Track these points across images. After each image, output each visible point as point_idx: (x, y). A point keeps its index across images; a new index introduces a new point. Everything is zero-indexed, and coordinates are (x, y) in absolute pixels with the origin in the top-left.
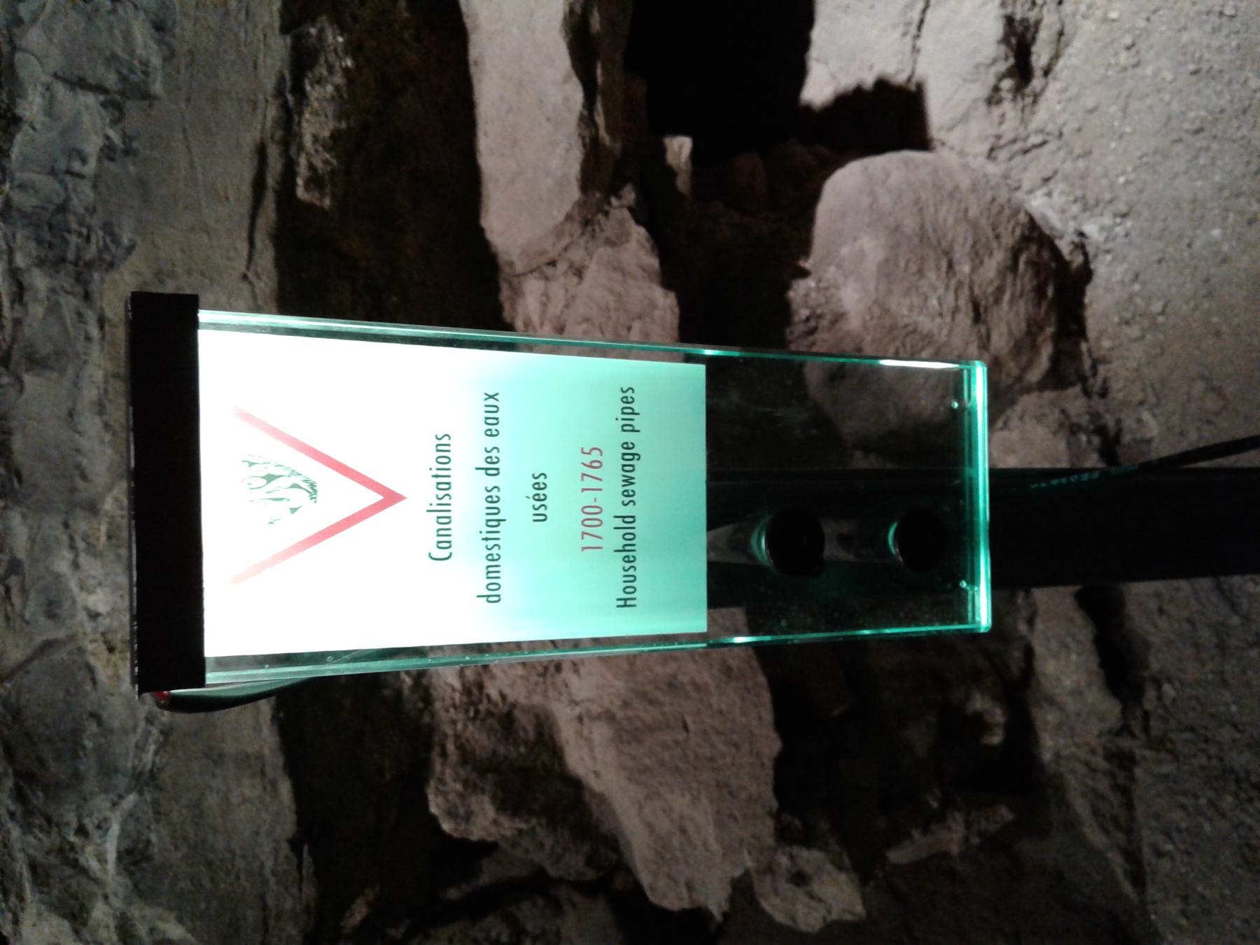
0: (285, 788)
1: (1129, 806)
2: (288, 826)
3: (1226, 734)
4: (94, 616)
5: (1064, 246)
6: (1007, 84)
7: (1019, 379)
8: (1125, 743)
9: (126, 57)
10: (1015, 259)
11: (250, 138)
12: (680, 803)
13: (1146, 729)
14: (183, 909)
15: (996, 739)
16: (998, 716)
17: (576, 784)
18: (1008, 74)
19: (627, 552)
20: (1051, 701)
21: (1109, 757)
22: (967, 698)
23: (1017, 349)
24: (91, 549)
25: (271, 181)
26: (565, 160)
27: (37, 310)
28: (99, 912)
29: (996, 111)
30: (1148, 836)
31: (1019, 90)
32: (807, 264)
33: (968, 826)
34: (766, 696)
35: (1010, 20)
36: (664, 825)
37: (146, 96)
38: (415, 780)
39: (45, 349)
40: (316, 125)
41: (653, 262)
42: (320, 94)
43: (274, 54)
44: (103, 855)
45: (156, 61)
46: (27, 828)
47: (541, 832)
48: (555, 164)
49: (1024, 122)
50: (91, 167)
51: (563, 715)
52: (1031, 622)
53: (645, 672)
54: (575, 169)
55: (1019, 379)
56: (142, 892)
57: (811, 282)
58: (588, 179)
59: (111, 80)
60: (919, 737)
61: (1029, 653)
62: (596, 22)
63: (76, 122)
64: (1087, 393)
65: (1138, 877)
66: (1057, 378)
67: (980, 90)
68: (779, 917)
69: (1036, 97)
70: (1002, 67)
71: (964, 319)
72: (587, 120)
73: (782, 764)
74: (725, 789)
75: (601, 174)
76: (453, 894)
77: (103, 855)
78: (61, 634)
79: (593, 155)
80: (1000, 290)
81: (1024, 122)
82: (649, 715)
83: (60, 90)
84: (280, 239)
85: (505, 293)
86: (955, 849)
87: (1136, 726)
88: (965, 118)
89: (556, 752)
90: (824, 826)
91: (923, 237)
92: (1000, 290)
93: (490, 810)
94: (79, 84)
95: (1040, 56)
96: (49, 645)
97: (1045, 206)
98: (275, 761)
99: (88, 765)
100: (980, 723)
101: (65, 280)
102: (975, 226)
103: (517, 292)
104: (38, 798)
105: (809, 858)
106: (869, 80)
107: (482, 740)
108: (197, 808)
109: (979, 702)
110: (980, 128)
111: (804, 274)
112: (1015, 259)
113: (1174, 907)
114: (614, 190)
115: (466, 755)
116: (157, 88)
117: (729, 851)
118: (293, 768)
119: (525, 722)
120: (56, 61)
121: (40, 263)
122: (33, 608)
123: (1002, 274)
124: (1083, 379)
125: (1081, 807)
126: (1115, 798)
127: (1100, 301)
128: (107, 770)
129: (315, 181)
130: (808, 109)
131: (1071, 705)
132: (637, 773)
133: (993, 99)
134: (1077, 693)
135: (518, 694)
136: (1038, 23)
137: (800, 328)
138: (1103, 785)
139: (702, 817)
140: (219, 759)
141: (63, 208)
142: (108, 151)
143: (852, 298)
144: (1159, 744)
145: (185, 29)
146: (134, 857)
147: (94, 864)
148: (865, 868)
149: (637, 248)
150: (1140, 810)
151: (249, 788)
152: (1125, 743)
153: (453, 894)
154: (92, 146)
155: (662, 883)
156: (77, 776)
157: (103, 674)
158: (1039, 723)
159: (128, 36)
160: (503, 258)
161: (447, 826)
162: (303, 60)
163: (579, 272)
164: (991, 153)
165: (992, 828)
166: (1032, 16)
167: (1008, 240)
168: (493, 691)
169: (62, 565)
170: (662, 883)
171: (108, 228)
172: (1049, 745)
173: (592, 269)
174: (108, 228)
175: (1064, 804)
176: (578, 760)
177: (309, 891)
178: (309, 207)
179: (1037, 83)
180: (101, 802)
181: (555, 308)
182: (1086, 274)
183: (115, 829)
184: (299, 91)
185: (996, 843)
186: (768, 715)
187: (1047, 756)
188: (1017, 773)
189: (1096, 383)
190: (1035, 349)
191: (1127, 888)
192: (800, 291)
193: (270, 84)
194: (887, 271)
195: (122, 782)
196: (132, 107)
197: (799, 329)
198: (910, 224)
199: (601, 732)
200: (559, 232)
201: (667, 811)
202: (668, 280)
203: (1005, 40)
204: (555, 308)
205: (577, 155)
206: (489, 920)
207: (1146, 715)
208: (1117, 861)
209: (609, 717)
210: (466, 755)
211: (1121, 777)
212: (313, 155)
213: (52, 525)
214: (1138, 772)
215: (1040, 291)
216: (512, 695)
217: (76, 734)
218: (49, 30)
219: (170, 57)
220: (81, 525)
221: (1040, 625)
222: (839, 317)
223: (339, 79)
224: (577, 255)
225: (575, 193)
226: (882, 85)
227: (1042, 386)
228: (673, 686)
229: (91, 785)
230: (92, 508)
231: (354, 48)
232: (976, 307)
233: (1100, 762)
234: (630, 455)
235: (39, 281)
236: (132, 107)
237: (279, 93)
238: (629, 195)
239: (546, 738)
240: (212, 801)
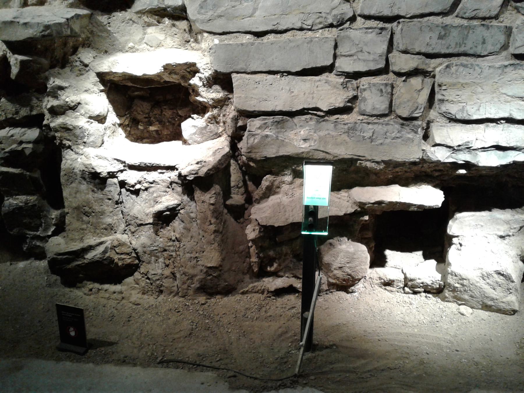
0: (274, 156)
1: (255, 292)
2: (268, 156)
3: (268, 307)
4: (300, 132)
5: (353, 288)
6: (383, 281)
7: (330, 277)
8: (266, 293)
9: (211, 277)
10: (349, 275)
11: (366, 155)
12: (269, 212)
13: (268, 297)
14: (259, 142)
15: (269, 269)
16: (273, 269)
17: (268, 197)
18: (384, 281)
19: (312, 198)
20: (273, 280)
21: (264, 289)
22: (276, 263)
23: (334, 275)
24: (309, 132)
25: (360, 158)
26: (363, 200)
27: (342, 126)
28: (259, 131)
29: (378, 279)
30: (249, 296)
31: (382, 283)
32: (350, 240)
33: (255, 262)
34: (283, 225)
35: (393, 281)
36: (265, 209)
37: (371, 142)
38: (270, 173)
39: (337, 127)
40: (369, 164)
41: (348, 213)
42: (373, 165)
43: (378, 159)
44: (267, 132)
45: (376, 143)
46: (272, 122)
47: (262, 192)
48: (363, 198)
49: (376, 284)
50: (362, 134)
51: (279, 196)
52: (287, 277)
53: (301, 198)
54: (361, 201)
55: (330, 277)
56: (262, 137)
57: (347, 240)
58: (360, 202)
59: (374, 137)
60: (271, 253)
61: (282, 277)
62: (383, 205)
63: (368, 132)
64: (326, 290)
65: (243, 293)
66: (330, 285)
67: (382, 276)
68: (247, 227)
69: (381, 287)
70: (385, 280)
71: (340, 265)
72: (369, 203)
73: (273, 227)
74: (270, 218)
75: (361, 205)
76: (247, 177)
77: (267, 132)
78: (298, 127)
79: (365, 204)
80: (344, 272)
81: (376, 284)
82: (282, 207)
83: (373, 130)
84: (352, 159)
85: (346, 190)
86: (251, 260)
87: (268, 295)
88: (377, 273)
89: (273, 195)
90: (261, 234)
91: (353, 258)
92: (344, 272)
93: (267, 184)
94: (373, 133)
95: (388, 288)
96: (296, 125)
97: (360, 286)
98: (278, 155)
99: (279, 130)
100: (271, 265)
101: (347, 130)
102: (355, 267)
103: (346, 192)
104: (276, 124)
105: (257, 232)
106: (387, 260)
107: (276, 183)
108: (273, 144)
109: (275, 265)
110: (375, 276)
111: (348, 240)
112: (349, 275)
113: (239, 298)
114: (360, 207)
115: (274, 181)
116: (373, 143)
117: (261, 218)
118: (276, 157)
119: (278, 190)
120: (377, 130)
121: (349, 127)
122: (301, 124)
123: (347, 272)
124: (329, 290)
125: (256, 284)
126: (257, 290)
127: (342, 294)
128: (278, 132)
129: (360, 164)
130: (384, 250)
131: (273, 283)
132: (273, 205)
133: (380, 278)
134: (275, 284)
135: (282, 189)
136: (393, 287)
137: (339, 239)
138: (259, 288)
139: (266, 215)
140: (279, 147)
141: (356, 130)
142: (364, 137)
143: (344, 247)
144: (266, 298)
145: (381, 147)
146: (267, 136)
147: (266, 130)
148: (253, 241)
149: (351, 210)
150: (255, 294)
151: (274, 151)
152: (266, 293)
153: (247, 177)
154: (365, 135)
155: (256, 209)
156: (278, 128)
157: (292, 132)
158: (269, 278)
159: (380, 140)
160: (351, 190)
161: (265, 178)
162: (378, 163)
163: (348, 201)
164: (370, 278)
165: (254, 268)
166: (395, 286)
167: (352, 274)
168: (283, 185)
169: (307, 128)
170: (256, 209)
171: (353, 136)
172: (266, 280)
173: (348, 203)
174: (353, 136)
175: (256, 282)
176: (272, 198)
177: (259, 159)
178: (357, 162)
179: (383, 287)
180: (274, 131)
181: (343, 198)
182: (348, 292)
183: (271, 134)
184: (373, 162)
185: (250, 267)
186: (280, 225)
187: (264, 279)
188: (262, 273)
189: (328, 292)
190: (334, 279)
191: (242, 291)
192: (345, 239)
193: (374, 158)
194: (347, 252)
195: (277, 134)
196: (370, 140)
197: (339, 239)
198: (355, 257)
199: (279, 201)
200: (353, 198)
201: (267, 210)
202: (345, 215)
203: (390, 280)
204: (343, 198)
205: (364, 201)
206: (242, 183)
207: (270, 297)
208: (246, 289)
209: (281, 202)
210: (274, 181)
211: (260, 291)
212: (364, 164)
213: (313, 127)
214: (261, 295)
215: (344, 280)
216: (282, 188)
217: (283, 128)
218: (381, 129)
219: (377, 145)
220: (313, 131)
221: (287, 278)
222: (340, 245)
223: (375, 167)
224: (350, 201)
225: (358, 201)
226: (386, 262)
227: (328, 281)
228: (285, 211)
229: (277, 130)
230: (315, 132)
231: (381, 170)
232: (341, 267)
233: (263, 288)
234: (320, 199)
235: (346, 127)
236: (370, 140)
237: (373, 159)
238: (359, 209)
239: (275, 193)
240: (273, 146)
